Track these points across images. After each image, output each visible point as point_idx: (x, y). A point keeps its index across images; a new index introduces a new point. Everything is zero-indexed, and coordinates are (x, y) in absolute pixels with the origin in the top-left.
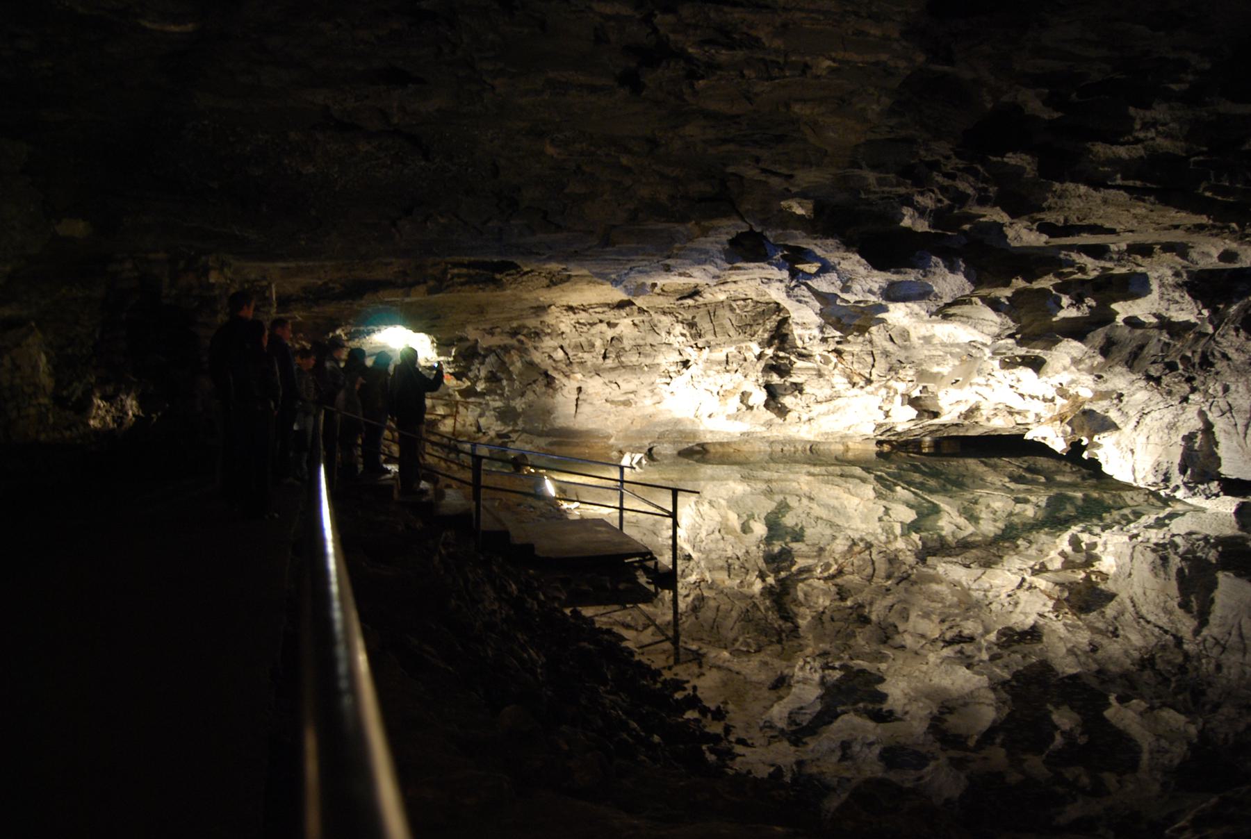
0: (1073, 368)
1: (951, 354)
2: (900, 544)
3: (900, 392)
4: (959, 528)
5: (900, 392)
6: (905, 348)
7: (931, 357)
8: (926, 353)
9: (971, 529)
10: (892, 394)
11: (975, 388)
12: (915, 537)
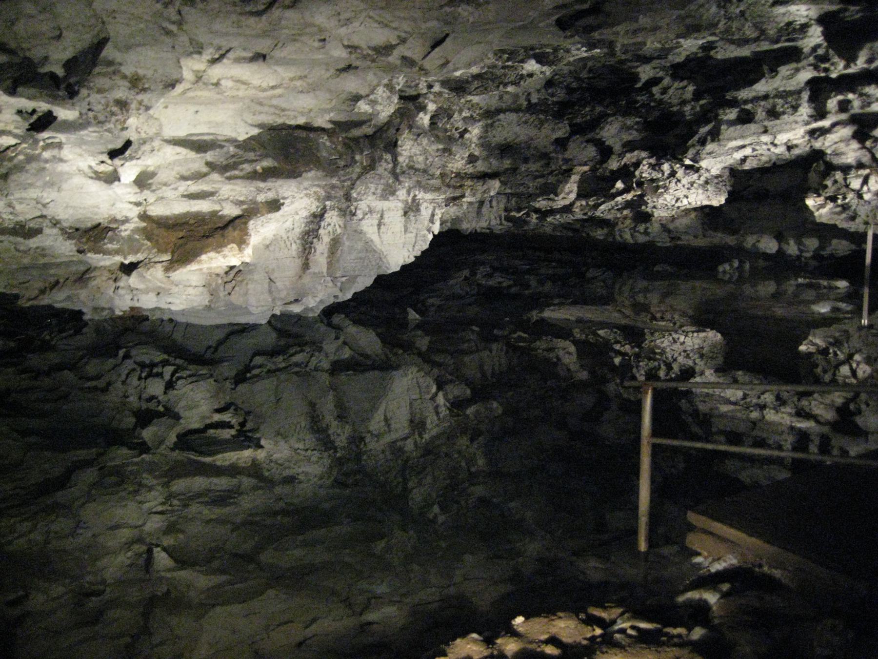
0: (215, 176)
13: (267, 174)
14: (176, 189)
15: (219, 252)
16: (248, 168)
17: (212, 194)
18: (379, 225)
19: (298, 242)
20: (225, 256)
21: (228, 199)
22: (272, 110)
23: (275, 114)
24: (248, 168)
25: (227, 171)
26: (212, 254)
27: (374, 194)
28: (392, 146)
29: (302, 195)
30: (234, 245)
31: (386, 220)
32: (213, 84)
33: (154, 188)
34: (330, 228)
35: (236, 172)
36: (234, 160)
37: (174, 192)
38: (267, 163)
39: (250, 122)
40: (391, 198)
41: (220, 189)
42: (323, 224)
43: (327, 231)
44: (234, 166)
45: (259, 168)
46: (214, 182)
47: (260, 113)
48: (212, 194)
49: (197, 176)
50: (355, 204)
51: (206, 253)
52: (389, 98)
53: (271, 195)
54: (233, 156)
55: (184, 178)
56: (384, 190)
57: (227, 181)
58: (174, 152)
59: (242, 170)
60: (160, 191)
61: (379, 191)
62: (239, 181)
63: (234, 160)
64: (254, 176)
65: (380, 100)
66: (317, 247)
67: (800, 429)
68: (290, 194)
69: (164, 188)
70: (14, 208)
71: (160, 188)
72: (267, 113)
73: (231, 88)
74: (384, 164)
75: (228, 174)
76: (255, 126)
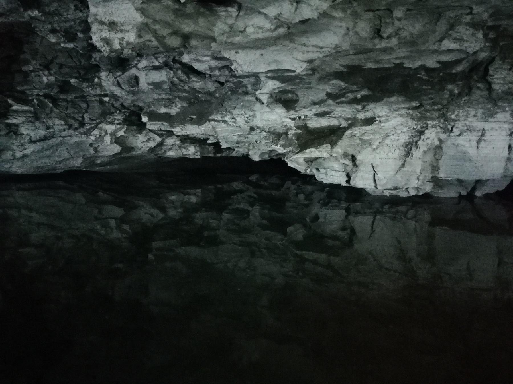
0: (330, 102)
1: (179, 98)
2: (116, 234)
3: (109, 131)
4: (152, 215)
5: (109, 131)
6: (133, 93)
7: (159, 100)
8: (156, 96)
9: (161, 216)
10: (103, 134)
11: (212, 123)
12: (126, 227)
13: (364, 100)
14: (311, 110)
15: (317, 149)
16: (350, 96)
17: (329, 113)
18: (479, 142)
19: (402, 148)
20: (319, 152)
21: (341, 116)
22: (315, 49)
23: (317, 52)
24: (350, 96)
25: (338, 98)
26: (313, 149)
27: (474, 116)
28: (485, 77)
29: (394, 115)
30: (329, 145)
31: (487, 137)
32: (240, 32)
33: (297, 109)
34: (429, 141)
35: (344, 99)
36: (344, 91)
37: (310, 112)
38: (364, 92)
39: (301, 59)
40: (490, 120)
41: (334, 110)
42: (422, 137)
43: (425, 143)
44: (343, 96)
45: (359, 96)
46: (329, 105)
47: (308, 52)
48: (329, 113)
49: (320, 103)
50: (452, 123)
51: (309, 148)
52: (473, 34)
53: (369, 114)
54: (344, 89)
55: (314, 103)
56: (483, 113)
57: (338, 105)
58: (273, 84)
59: (347, 98)
60: (302, 111)
61: (479, 115)
62: (345, 105)
63: (344, 91)
64: (355, 101)
65: (465, 37)
66: (414, 153)
67: (296, 253)
68: (384, 114)
69: (304, 109)
70: (236, 119)
71: (301, 110)
72: (313, 52)
73: (254, 33)
74: (478, 92)
75: (339, 100)
76: (305, 61)
